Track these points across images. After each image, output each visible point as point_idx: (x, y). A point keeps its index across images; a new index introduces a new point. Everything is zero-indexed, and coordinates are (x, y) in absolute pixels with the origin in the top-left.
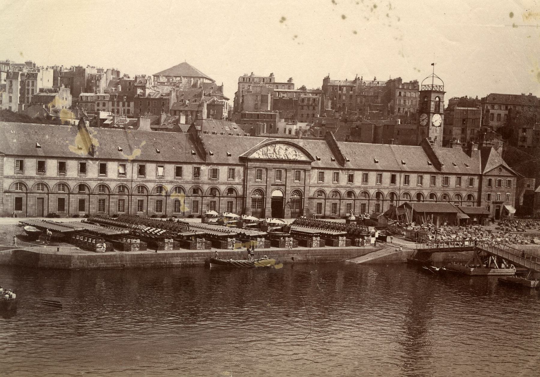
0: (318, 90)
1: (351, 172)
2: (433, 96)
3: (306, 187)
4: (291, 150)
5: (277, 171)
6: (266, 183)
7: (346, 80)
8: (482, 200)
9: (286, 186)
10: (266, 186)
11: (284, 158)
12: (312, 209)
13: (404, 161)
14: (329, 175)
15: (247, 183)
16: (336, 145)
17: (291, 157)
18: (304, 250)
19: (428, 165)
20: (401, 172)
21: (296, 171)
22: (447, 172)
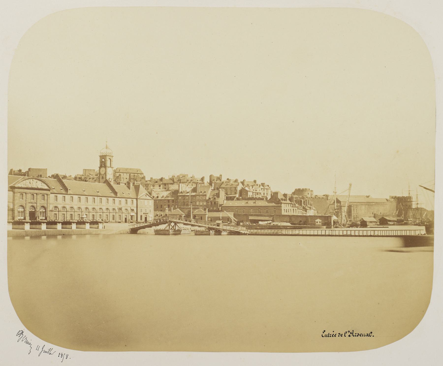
3: (48, 204)
4: (39, 182)
5: (32, 194)
6: (26, 202)
7: (255, 181)
9: (37, 204)
10: (26, 203)
11: (35, 187)
12: (52, 217)
13: (84, 189)
15: (15, 201)
16: (62, 181)
17: (40, 187)
18: (386, 225)
21: (42, 195)
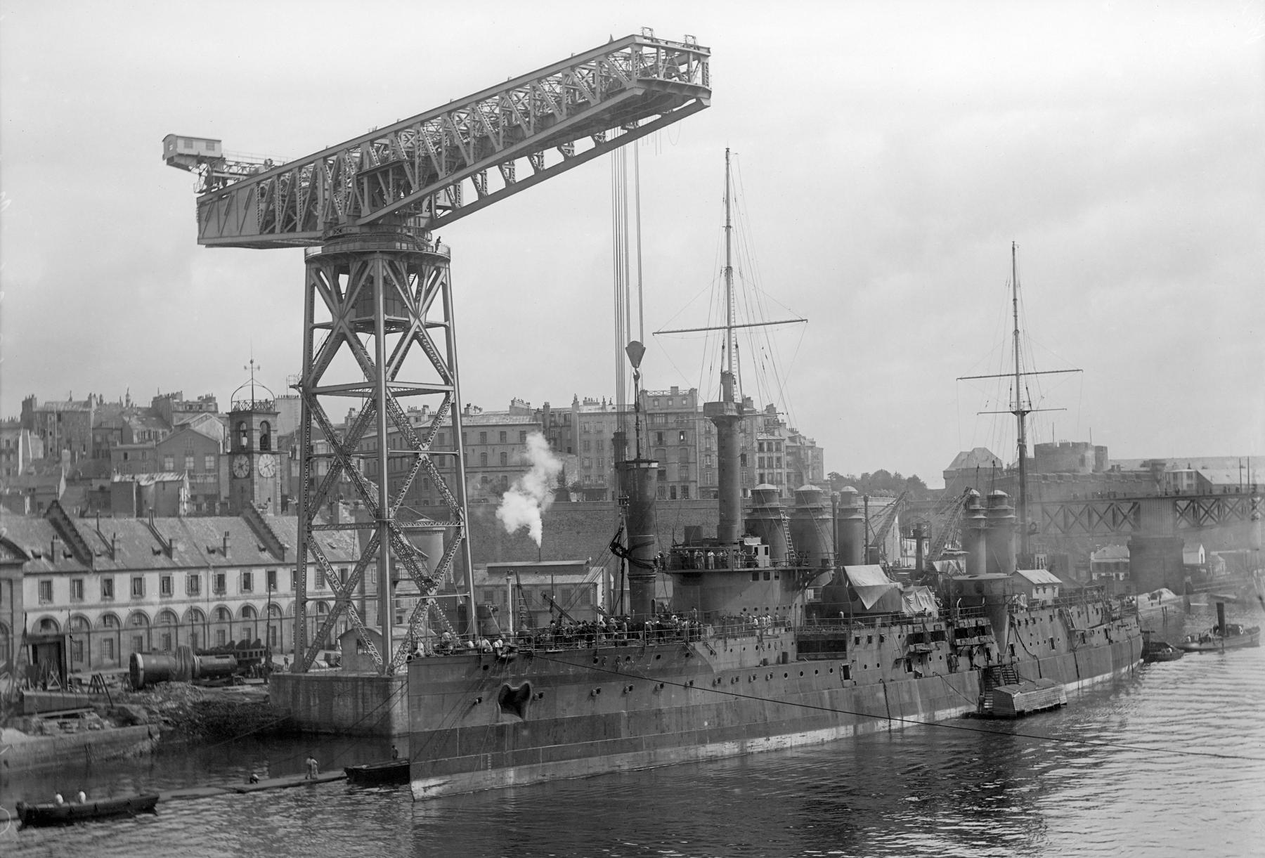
0: (13, 421)
1: (108, 576)
2: (256, 421)
3: (14, 615)
8: (366, 609)
14: (61, 586)
19: (258, 552)
20: (207, 568)
22: (237, 564)
